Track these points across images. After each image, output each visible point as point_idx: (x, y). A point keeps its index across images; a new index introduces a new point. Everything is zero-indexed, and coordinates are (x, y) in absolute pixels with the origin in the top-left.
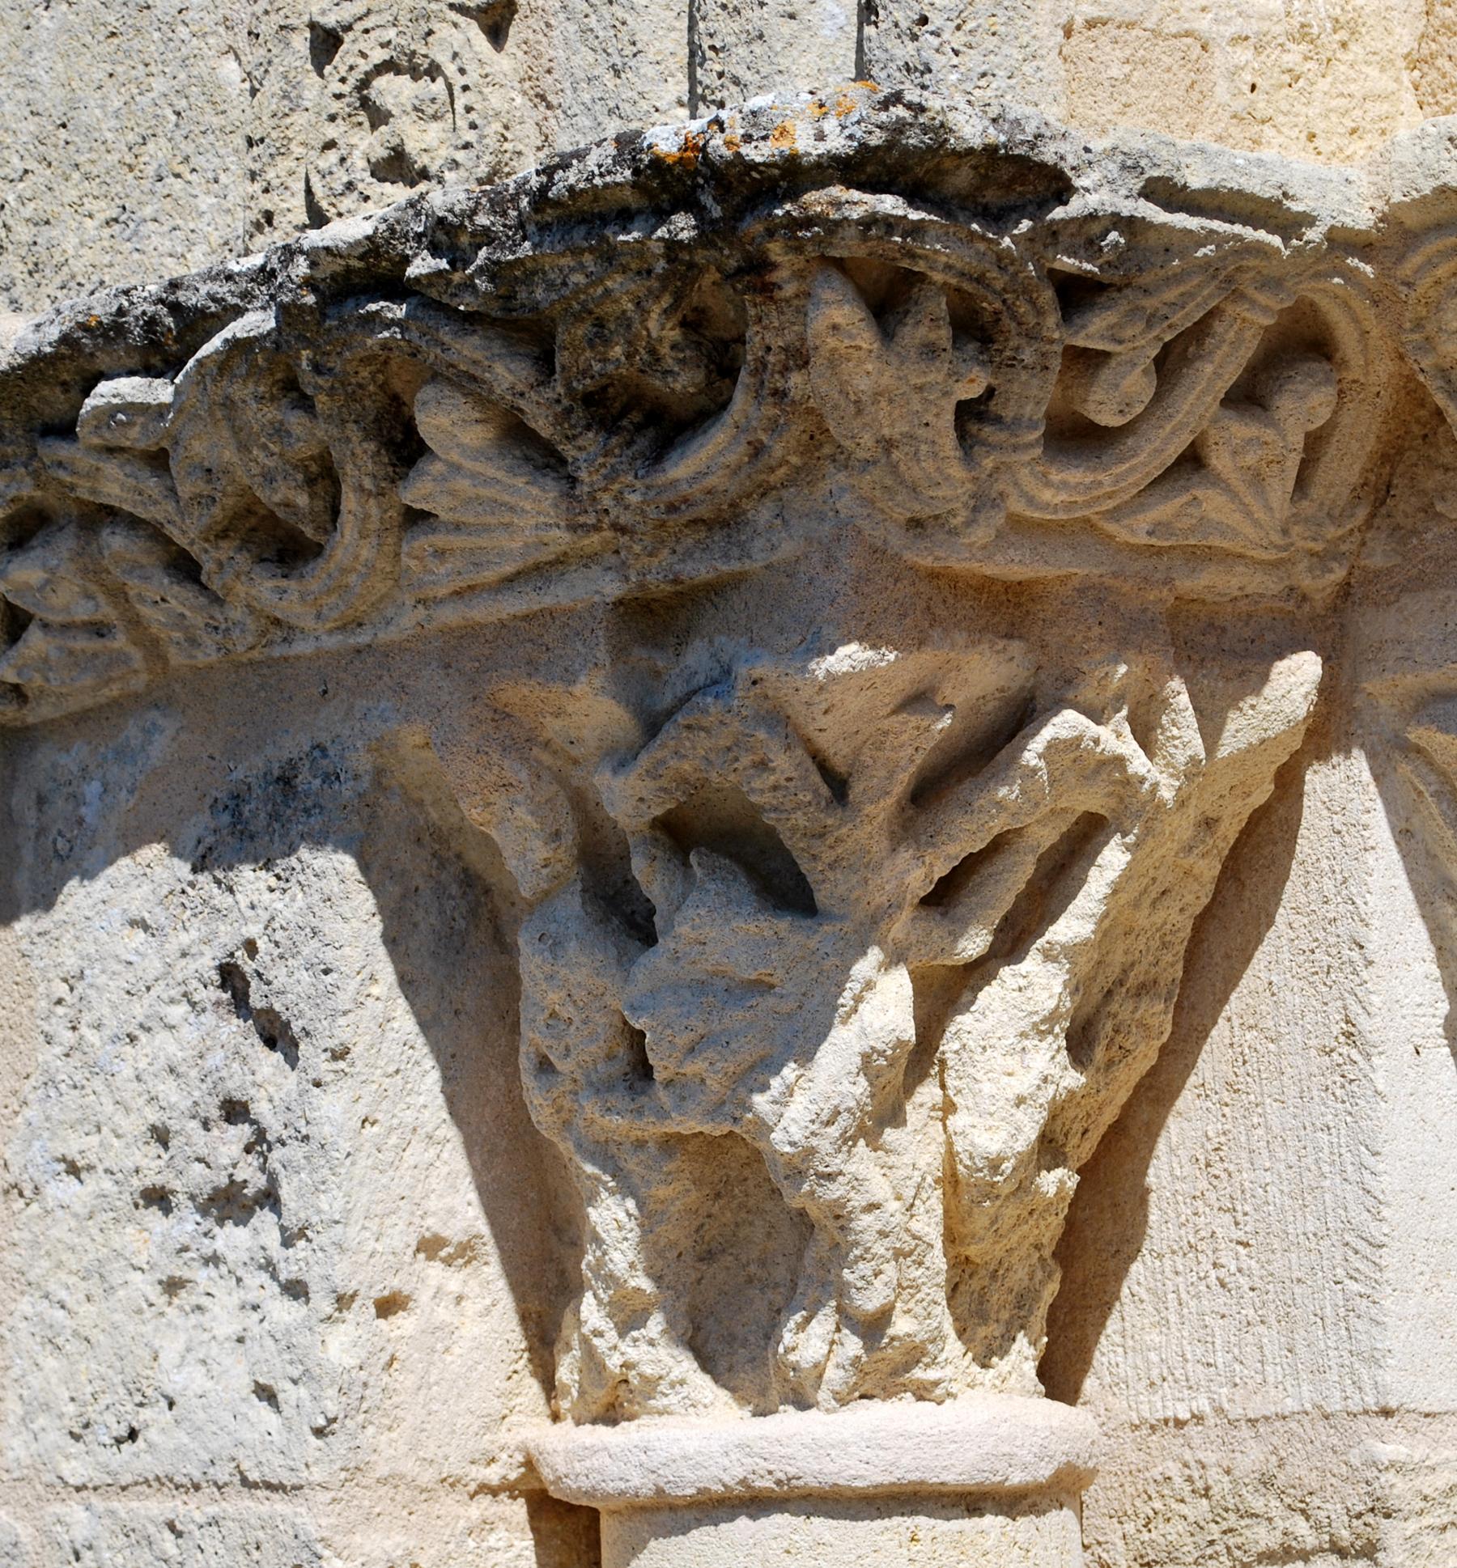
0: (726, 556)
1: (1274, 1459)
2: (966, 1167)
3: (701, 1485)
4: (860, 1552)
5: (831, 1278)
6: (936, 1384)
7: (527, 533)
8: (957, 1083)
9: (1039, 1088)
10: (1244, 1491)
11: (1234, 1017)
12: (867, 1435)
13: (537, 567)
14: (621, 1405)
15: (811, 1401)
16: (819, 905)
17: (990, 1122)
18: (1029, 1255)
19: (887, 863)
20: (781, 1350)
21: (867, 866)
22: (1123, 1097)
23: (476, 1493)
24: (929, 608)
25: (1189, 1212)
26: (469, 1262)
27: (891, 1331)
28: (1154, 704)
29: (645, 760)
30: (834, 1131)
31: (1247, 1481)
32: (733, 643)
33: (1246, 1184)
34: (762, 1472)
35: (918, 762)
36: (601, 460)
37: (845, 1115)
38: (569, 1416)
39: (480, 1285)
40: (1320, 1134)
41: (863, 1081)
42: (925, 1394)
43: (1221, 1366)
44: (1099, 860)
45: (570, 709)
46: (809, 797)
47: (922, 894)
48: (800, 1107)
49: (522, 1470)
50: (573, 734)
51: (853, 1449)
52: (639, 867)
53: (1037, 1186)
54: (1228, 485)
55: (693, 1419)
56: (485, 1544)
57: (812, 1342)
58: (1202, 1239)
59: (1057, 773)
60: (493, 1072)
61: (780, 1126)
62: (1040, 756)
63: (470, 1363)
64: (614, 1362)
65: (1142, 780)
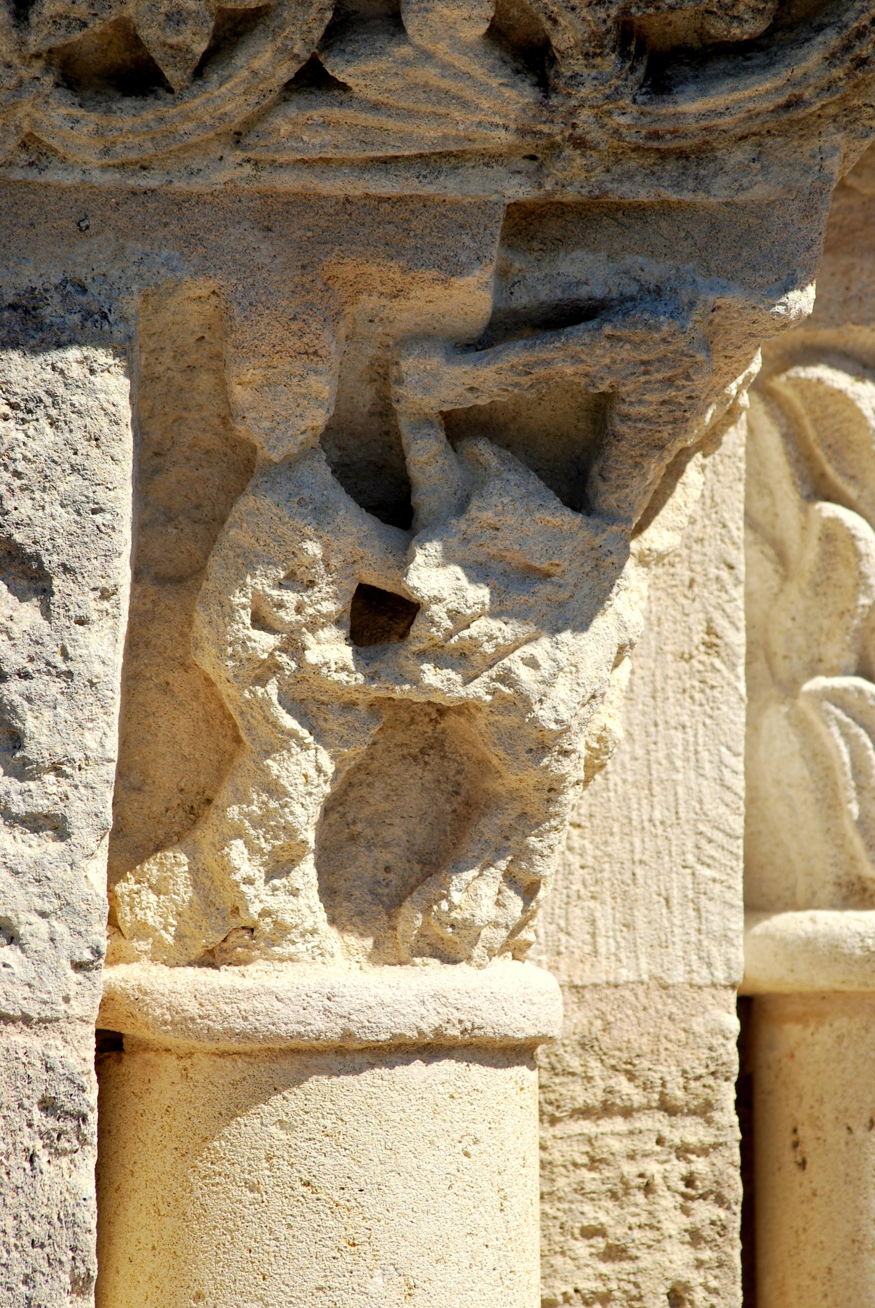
0: (677, 185)
3: (398, 1031)
10: (561, 1051)
31: (566, 1042)
40: (673, 732)
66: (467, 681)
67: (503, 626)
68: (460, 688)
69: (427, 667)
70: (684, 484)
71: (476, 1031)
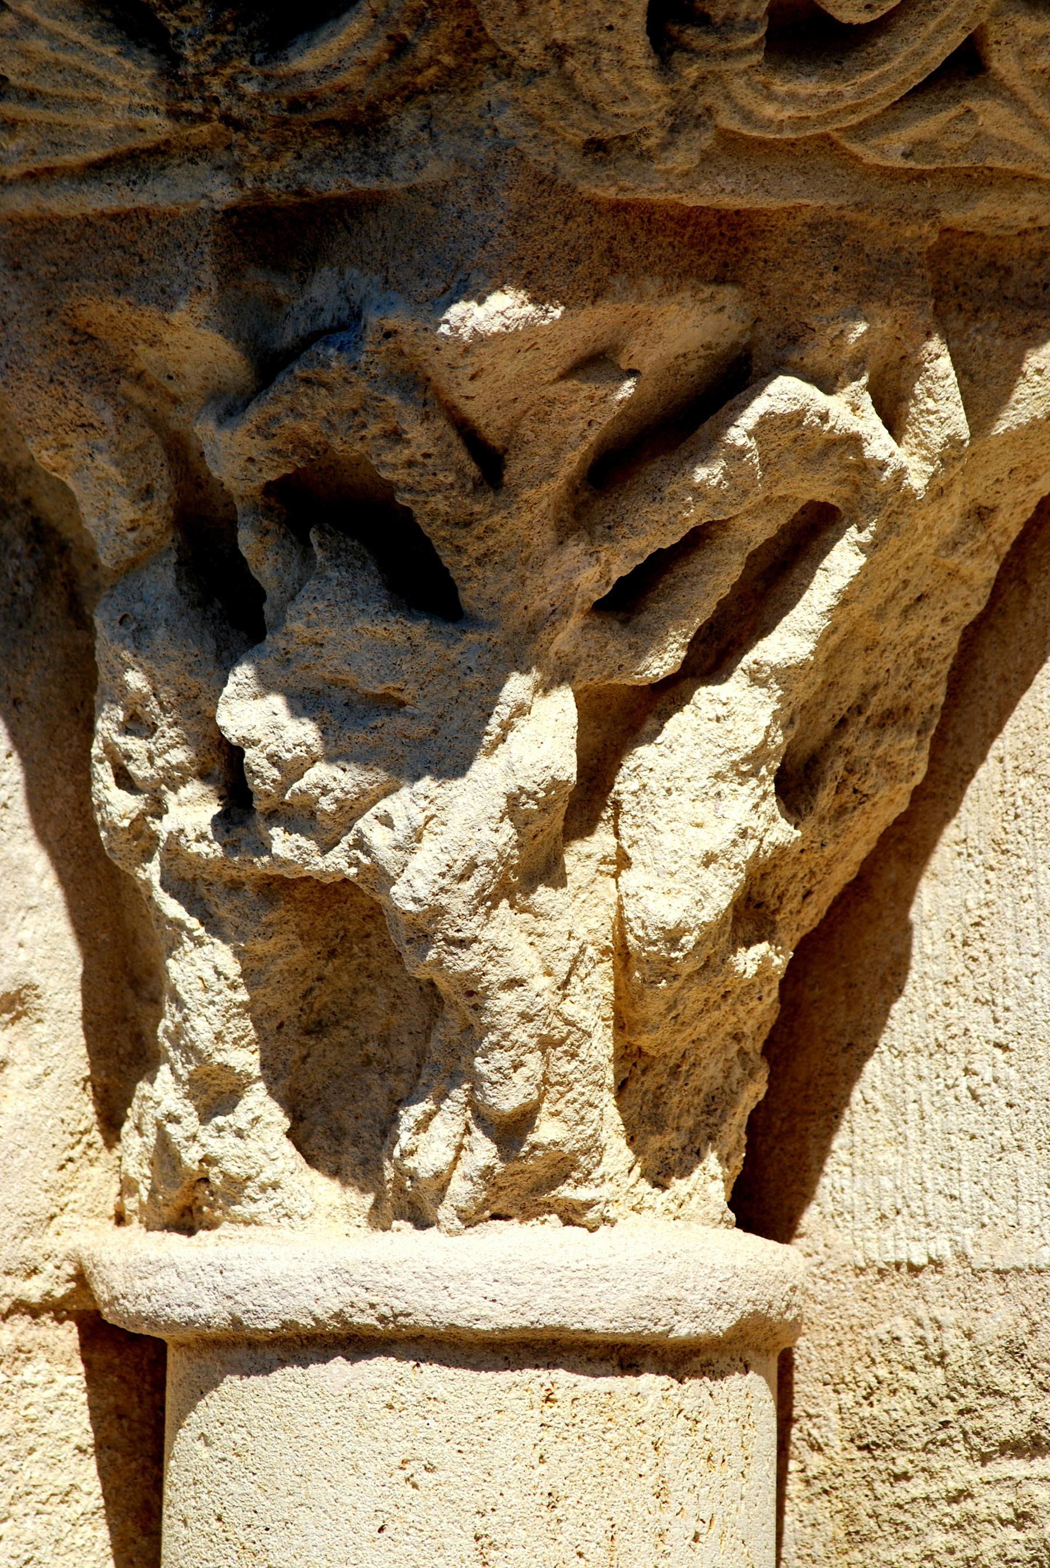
0: (361, 171)
1: (1025, 1322)
2: (637, 937)
3: (287, 1317)
4: (480, 1412)
5: (462, 1067)
6: (589, 1205)
7: (118, 114)
8: (634, 832)
9: (734, 843)
10: (986, 1362)
11: (1008, 758)
12: (496, 1265)
13: (133, 155)
14: (200, 1209)
15: (431, 1218)
16: (465, 607)
17: (670, 883)
18: (725, 1048)
19: (550, 559)
20: (396, 1153)
21: (525, 562)
22: (860, 851)
23: (10, 1312)
24: (610, 250)
25: (939, 1001)
26: (17, 1017)
27: (532, 1138)
28: (906, 370)
29: (255, 414)
30: (469, 888)
31: (991, 1348)
32: (366, 280)
33: (1010, 971)
34: (362, 1306)
35: (592, 439)
36: (209, 37)
37: (484, 869)
38: (136, 1219)
39: (30, 1048)
41: (508, 828)
42: (574, 1217)
43: (966, 1200)
44: (826, 563)
45: (167, 338)
46: (451, 479)
47: (596, 598)
48: (429, 856)
49: (73, 1285)
50: (172, 367)
51: (477, 1282)
52: (247, 540)
53: (731, 965)
54: (1014, 94)
55: (286, 1233)
56: (17, 1379)
57: (434, 1146)
58: (952, 1037)
59: (772, 455)
60: (59, 779)
61: (404, 877)
62: (750, 434)
63: (11, 1146)
64: (191, 1156)
65: (883, 466)
66: (325, 849)
67: (340, 774)
68: (318, 859)
69: (276, 832)
70: (825, 570)
71: (401, 1319)
